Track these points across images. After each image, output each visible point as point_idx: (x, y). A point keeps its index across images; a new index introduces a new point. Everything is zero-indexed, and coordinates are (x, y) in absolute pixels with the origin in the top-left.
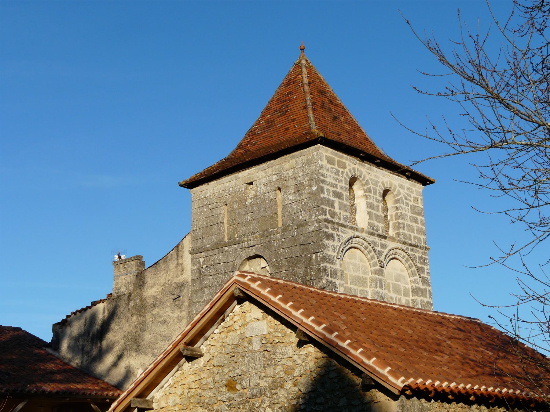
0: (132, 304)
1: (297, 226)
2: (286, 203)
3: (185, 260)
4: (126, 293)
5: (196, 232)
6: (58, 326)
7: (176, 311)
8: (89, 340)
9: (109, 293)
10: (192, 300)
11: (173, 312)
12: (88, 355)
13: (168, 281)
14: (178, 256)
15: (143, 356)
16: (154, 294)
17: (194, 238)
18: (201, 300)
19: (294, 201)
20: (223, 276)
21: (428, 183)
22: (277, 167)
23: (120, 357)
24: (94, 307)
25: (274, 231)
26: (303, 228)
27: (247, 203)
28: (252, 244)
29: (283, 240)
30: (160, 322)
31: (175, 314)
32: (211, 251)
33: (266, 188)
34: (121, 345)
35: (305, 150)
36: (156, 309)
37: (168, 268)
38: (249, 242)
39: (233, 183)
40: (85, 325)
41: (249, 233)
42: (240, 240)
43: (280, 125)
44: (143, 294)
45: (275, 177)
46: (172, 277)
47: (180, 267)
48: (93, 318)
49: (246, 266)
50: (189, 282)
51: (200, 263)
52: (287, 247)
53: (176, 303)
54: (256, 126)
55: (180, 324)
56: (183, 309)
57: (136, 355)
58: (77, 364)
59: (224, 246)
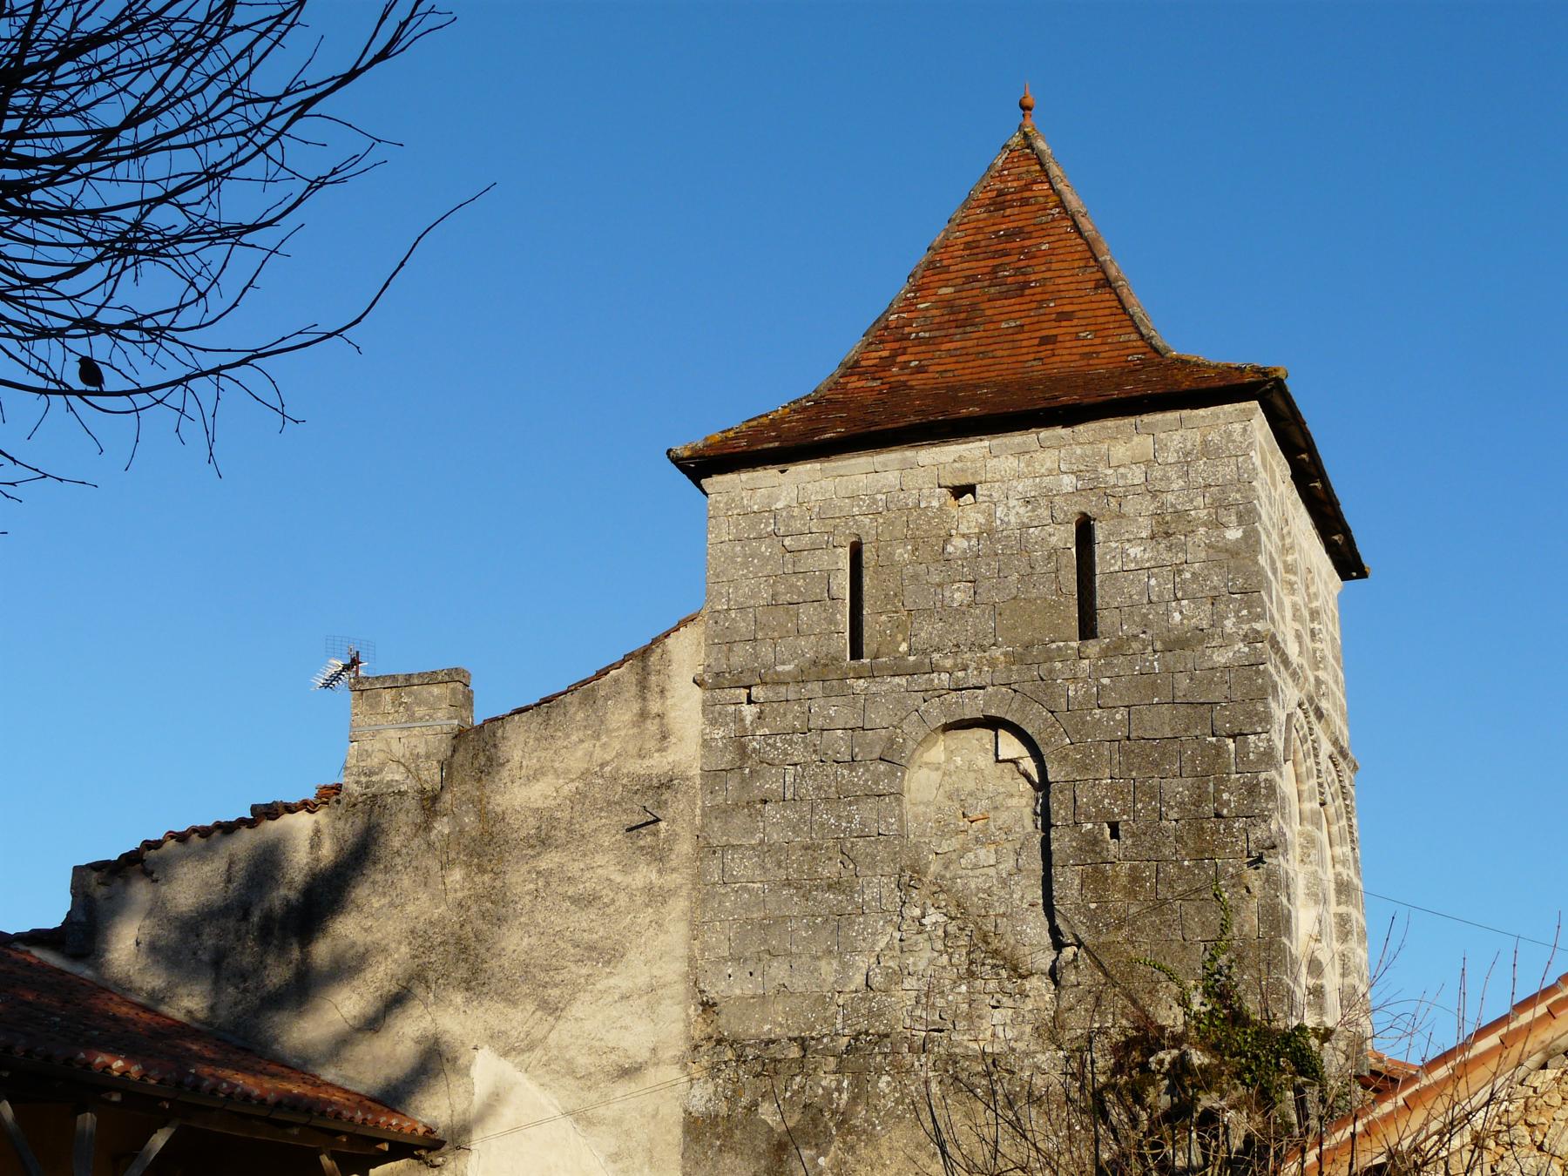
0: (442, 827)
1: (1164, 643)
2: (1117, 568)
3: (675, 705)
4: (403, 788)
5: (727, 620)
6: (95, 874)
7: (643, 868)
8: (248, 933)
9: (331, 782)
10: (705, 838)
11: (626, 869)
12: (242, 986)
13: (602, 766)
14: (643, 686)
15: (501, 1006)
16: (540, 804)
17: (717, 636)
18: (744, 841)
19: (1147, 565)
20: (846, 772)
21: (1354, 574)
22: (1079, 451)
23: (396, 1001)
24: (270, 822)
25: (1068, 647)
26: (1188, 653)
27: (950, 549)
28: (973, 682)
29: (1106, 681)
30: (570, 897)
31: (638, 876)
32: (792, 687)
33: (1033, 510)
34: (395, 961)
35: (1202, 412)
36: (553, 854)
37: (602, 722)
38: (961, 674)
39: (892, 478)
40: (229, 881)
41: (957, 646)
42: (922, 663)
43: (1018, 323)
44: (489, 797)
45: (1068, 482)
46: (618, 755)
47: (652, 727)
48: (268, 863)
49: (935, 749)
50: (692, 777)
51: (742, 720)
52: (1119, 703)
53: (642, 843)
54: (905, 315)
55: (657, 911)
56: (674, 864)
57: (468, 1001)
58: (189, 1012)
59: (851, 675)
